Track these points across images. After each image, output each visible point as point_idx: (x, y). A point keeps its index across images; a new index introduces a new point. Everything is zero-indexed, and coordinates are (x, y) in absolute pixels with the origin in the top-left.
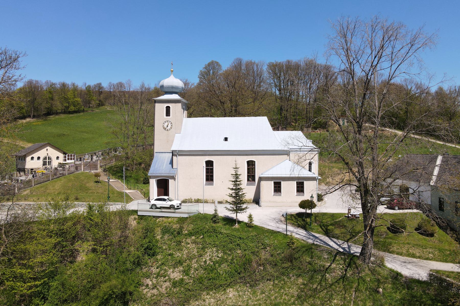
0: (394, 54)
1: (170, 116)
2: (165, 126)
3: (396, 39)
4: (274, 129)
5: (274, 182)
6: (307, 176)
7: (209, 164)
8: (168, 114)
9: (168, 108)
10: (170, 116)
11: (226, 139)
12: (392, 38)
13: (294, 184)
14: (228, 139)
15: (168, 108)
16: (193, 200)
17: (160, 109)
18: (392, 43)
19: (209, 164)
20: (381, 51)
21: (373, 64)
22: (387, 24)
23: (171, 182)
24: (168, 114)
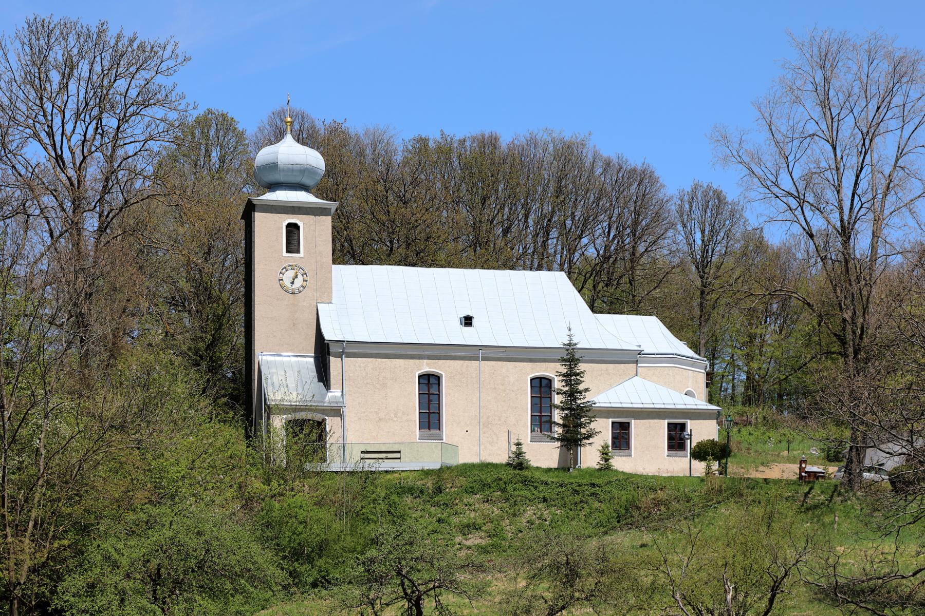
0: (908, 107)
1: (298, 252)
2: (287, 283)
3: (911, 81)
4: (593, 309)
5: (613, 423)
6: (695, 407)
7: (430, 382)
8: (293, 243)
9: (293, 229)
10: (298, 252)
11: (468, 321)
12: (904, 80)
13: (662, 426)
14: (474, 321)
15: (293, 229)
16: (674, 245)
17: (269, 230)
18: (904, 87)
19: (430, 382)
20: (888, 99)
21: (88, 136)
22: (898, 54)
23: (331, 423)
24: (293, 243)
